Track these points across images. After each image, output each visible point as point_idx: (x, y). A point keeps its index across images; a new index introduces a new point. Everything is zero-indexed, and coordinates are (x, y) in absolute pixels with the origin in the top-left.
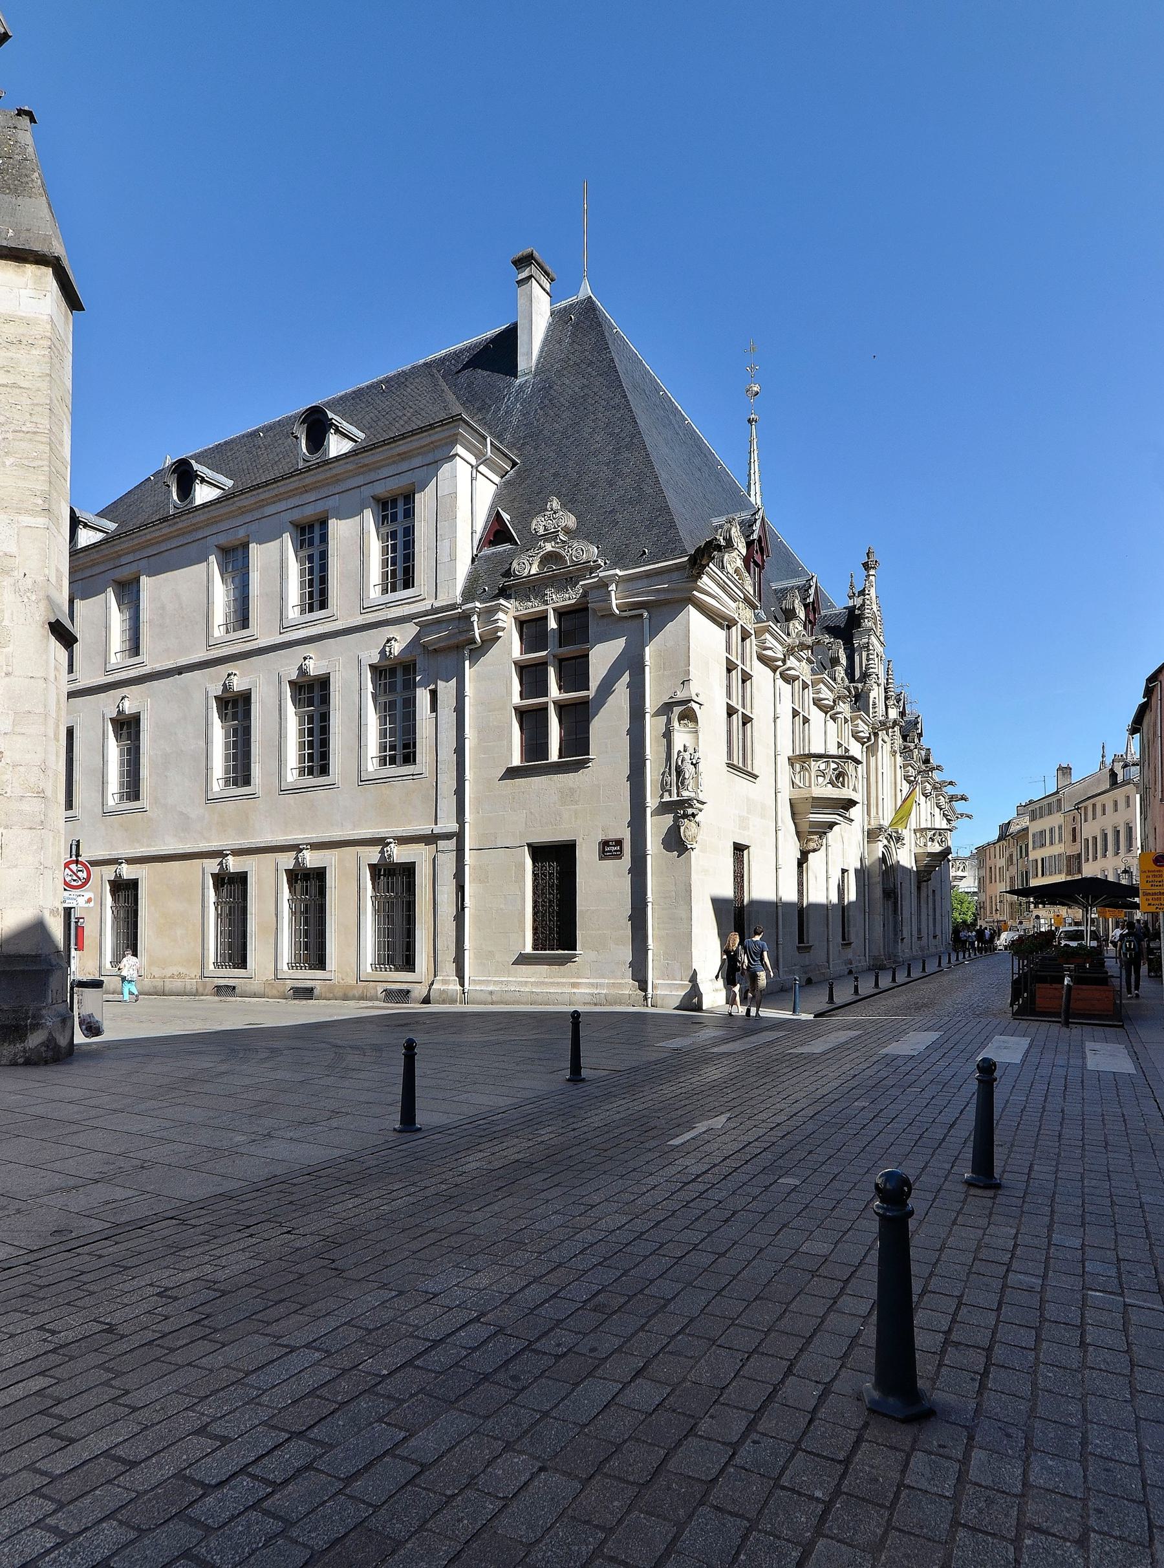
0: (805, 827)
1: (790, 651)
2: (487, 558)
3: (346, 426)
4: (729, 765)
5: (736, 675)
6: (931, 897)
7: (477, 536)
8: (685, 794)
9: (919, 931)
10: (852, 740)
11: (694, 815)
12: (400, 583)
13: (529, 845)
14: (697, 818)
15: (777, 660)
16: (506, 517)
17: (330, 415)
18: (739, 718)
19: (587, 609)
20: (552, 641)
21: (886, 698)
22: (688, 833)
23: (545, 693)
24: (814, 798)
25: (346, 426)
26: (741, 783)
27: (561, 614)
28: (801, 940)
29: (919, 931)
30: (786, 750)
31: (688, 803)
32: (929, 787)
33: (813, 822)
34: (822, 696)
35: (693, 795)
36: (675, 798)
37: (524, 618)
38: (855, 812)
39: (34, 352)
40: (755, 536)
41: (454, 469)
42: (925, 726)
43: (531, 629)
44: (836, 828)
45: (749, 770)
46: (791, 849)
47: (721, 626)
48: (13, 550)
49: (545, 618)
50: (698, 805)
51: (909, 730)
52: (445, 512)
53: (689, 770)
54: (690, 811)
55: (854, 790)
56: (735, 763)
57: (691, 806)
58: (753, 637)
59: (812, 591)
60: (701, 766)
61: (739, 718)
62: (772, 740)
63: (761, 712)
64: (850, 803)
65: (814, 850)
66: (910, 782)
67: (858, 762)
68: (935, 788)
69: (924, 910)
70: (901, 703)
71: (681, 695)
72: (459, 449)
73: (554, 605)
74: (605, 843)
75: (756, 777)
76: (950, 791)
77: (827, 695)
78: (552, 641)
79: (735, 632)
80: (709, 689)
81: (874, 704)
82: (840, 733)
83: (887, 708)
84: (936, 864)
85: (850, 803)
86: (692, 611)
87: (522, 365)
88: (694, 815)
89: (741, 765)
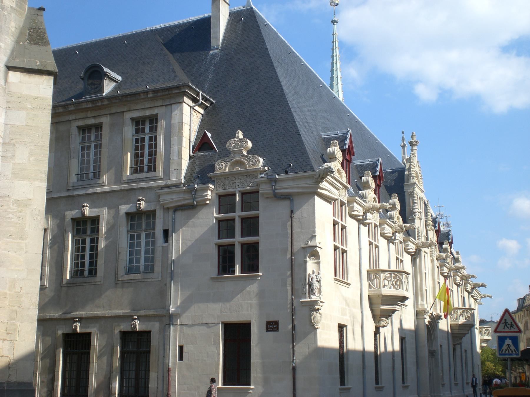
0: (378, 313)
1: (367, 211)
2: (199, 158)
3: (113, 74)
4: (335, 279)
5: (338, 228)
6: (463, 355)
7: (192, 144)
8: (314, 298)
9: (455, 380)
10: (405, 254)
11: (318, 309)
12: (146, 169)
13: (222, 323)
14: (320, 311)
15: (360, 216)
16: (209, 135)
17: (106, 69)
18: (341, 253)
19: (258, 192)
20: (238, 207)
21: (427, 225)
22: (316, 320)
23: (233, 236)
24: (383, 296)
25: (113, 74)
26: (342, 288)
27: (243, 194)
28: (377, 383)
29: (455, 380)
30: (366, 267)
31: (316, 302)
32: (458, 279)
33: (382, 308)
34: (385, 232)
35: (318, 298)
36: (308, 300)
37: (221, 194)
38: (410, 303)
39: (45, 112)
40: (347, 147)
41: (182, 110)
42: (455, 236)
43: (225, 202)
44: (396, 312)
45: (345, 281)
46: (370, 326)
47: (330, 203)
48: (31, 196)
49: (234, 195)
50: (321, 304)
51: (444, 239)
52: (174, 132)
53: (316, 285)
54: (317, 307)
55: (407, 290)
56: (338, 278)
57: (317, 305)
58: (346, 205)
59: (378, 168)
60: (321, 282)
61: (341, 253)
62: (357, 262)
63: (351, 247)
64: (404, 299)
65: (384, 326)
66: (444, 276)
67: (408, 274)
68: (462, 279)
69: (470, 365)
70: (437, 225)
71: (310, 244)
72: (186, 99)
73: (239, 189)
74: (268, 323)
75: (349, 284)
76: (474, 281)
77: (388, 231)
78: (238, 207)
79: (338, 204)
80: (324, 239)
81: (418, 231)
82: (397, 252)
83: (427, 231)
84: (463, 332)
85: (404, 299)
86: (317, 199)
87: (213, 43)
88: (318, 309)
89: (341, 279)
